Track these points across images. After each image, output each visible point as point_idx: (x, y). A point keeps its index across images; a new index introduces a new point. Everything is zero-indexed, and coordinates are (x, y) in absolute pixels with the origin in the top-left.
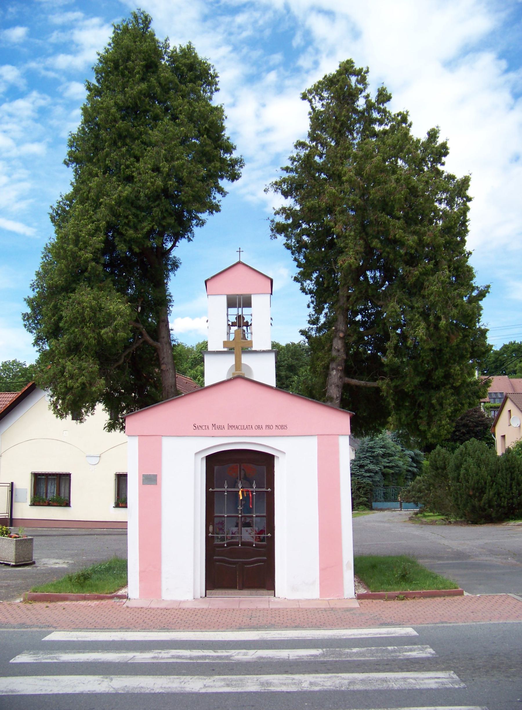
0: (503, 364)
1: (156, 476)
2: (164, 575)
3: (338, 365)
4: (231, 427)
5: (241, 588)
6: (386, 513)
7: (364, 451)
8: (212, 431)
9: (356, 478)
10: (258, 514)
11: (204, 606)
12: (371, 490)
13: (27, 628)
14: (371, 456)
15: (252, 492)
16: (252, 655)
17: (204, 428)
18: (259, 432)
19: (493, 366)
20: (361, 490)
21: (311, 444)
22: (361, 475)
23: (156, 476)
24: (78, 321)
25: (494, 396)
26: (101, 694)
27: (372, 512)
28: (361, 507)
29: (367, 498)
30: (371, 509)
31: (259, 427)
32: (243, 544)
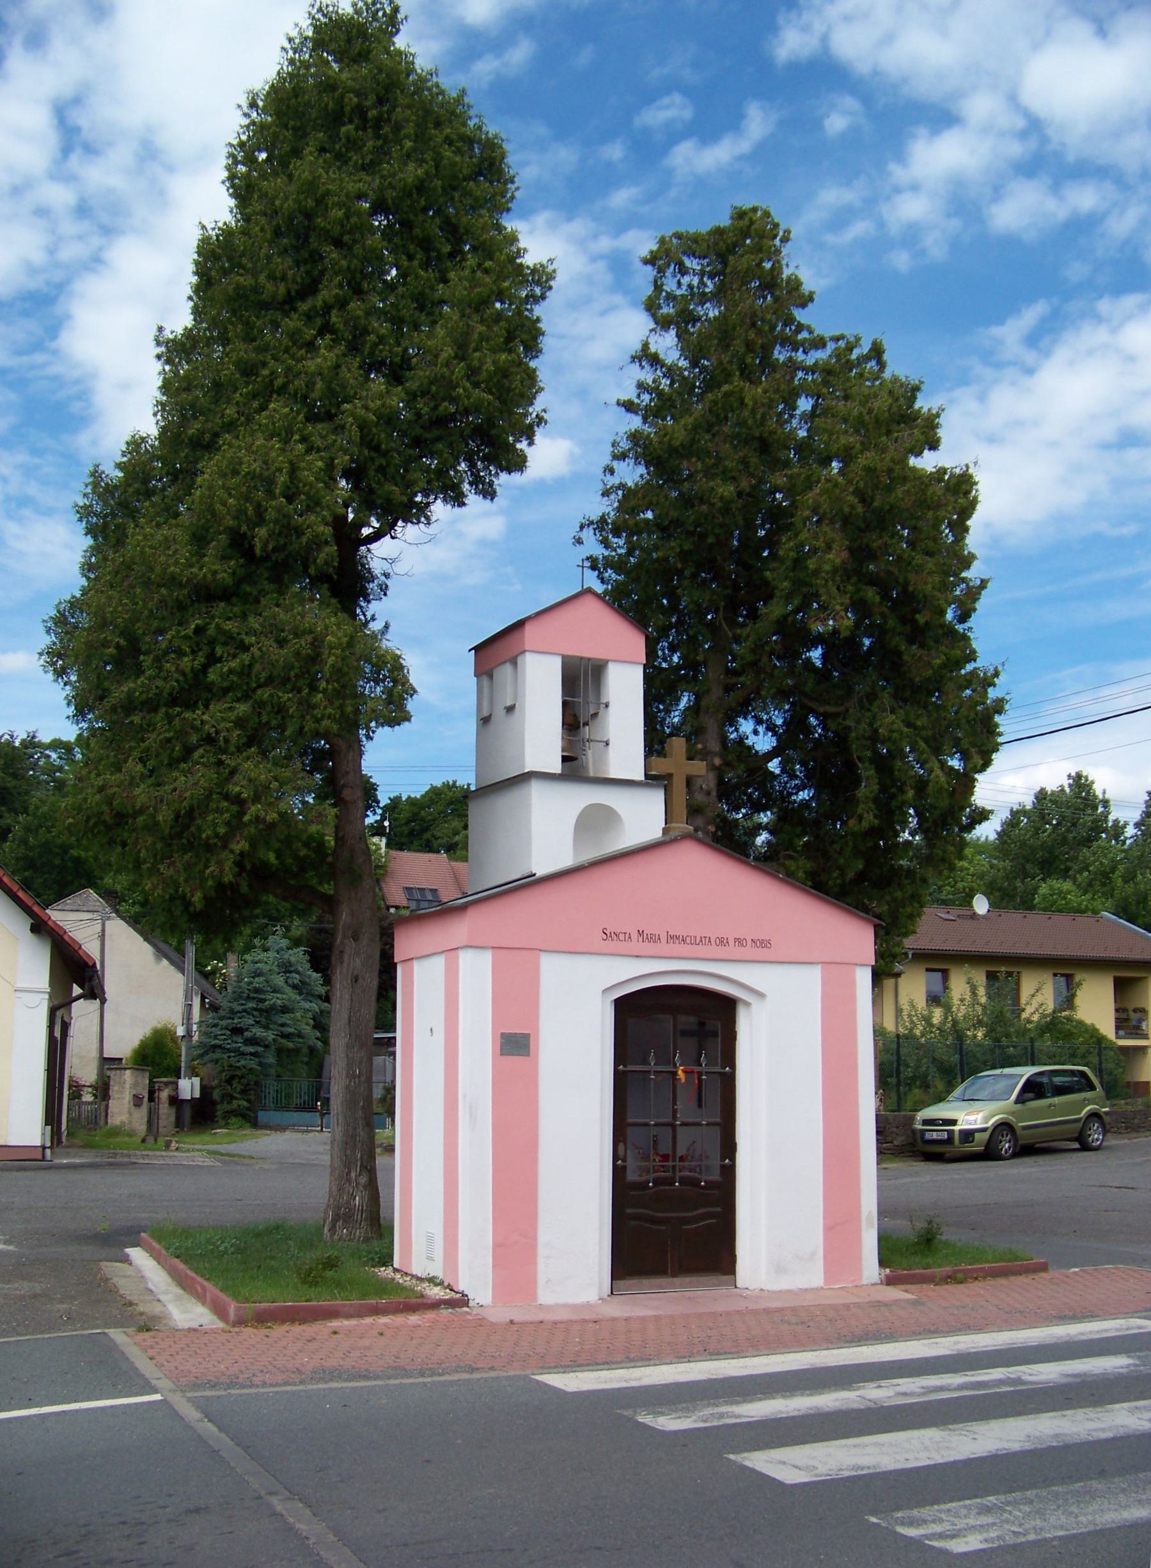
0: (427, 829)
1: (527, 1037)
2: (542, 1251)
3: (708, 823)
4: (672, 938)
5: (674, 1275)
6: (288, 1135)
7: (241, 997)
8: (637, 946)
9: (225, 1056)
10: (711, 1120)
11: (618, 1309)
12: (257, 1083)
13: (442, 1375)
14: (255, 1009)
15: (700, 1074)
16: (912, 1387)
17: (622, 937)
18: (721, 952)
19: (406, 830)
20: (235, 1083)
21: (810, 979)
22: (237, 1050)
23: (527, 1037)
24: (292, 673)
25: (418, 896)
26: (982, 1460)
27: (259, 1132)
28: (233, 1120)
29: (249, 1101)
30: (255, 1124)
31: (722, 942)
32: (683, 1181)
